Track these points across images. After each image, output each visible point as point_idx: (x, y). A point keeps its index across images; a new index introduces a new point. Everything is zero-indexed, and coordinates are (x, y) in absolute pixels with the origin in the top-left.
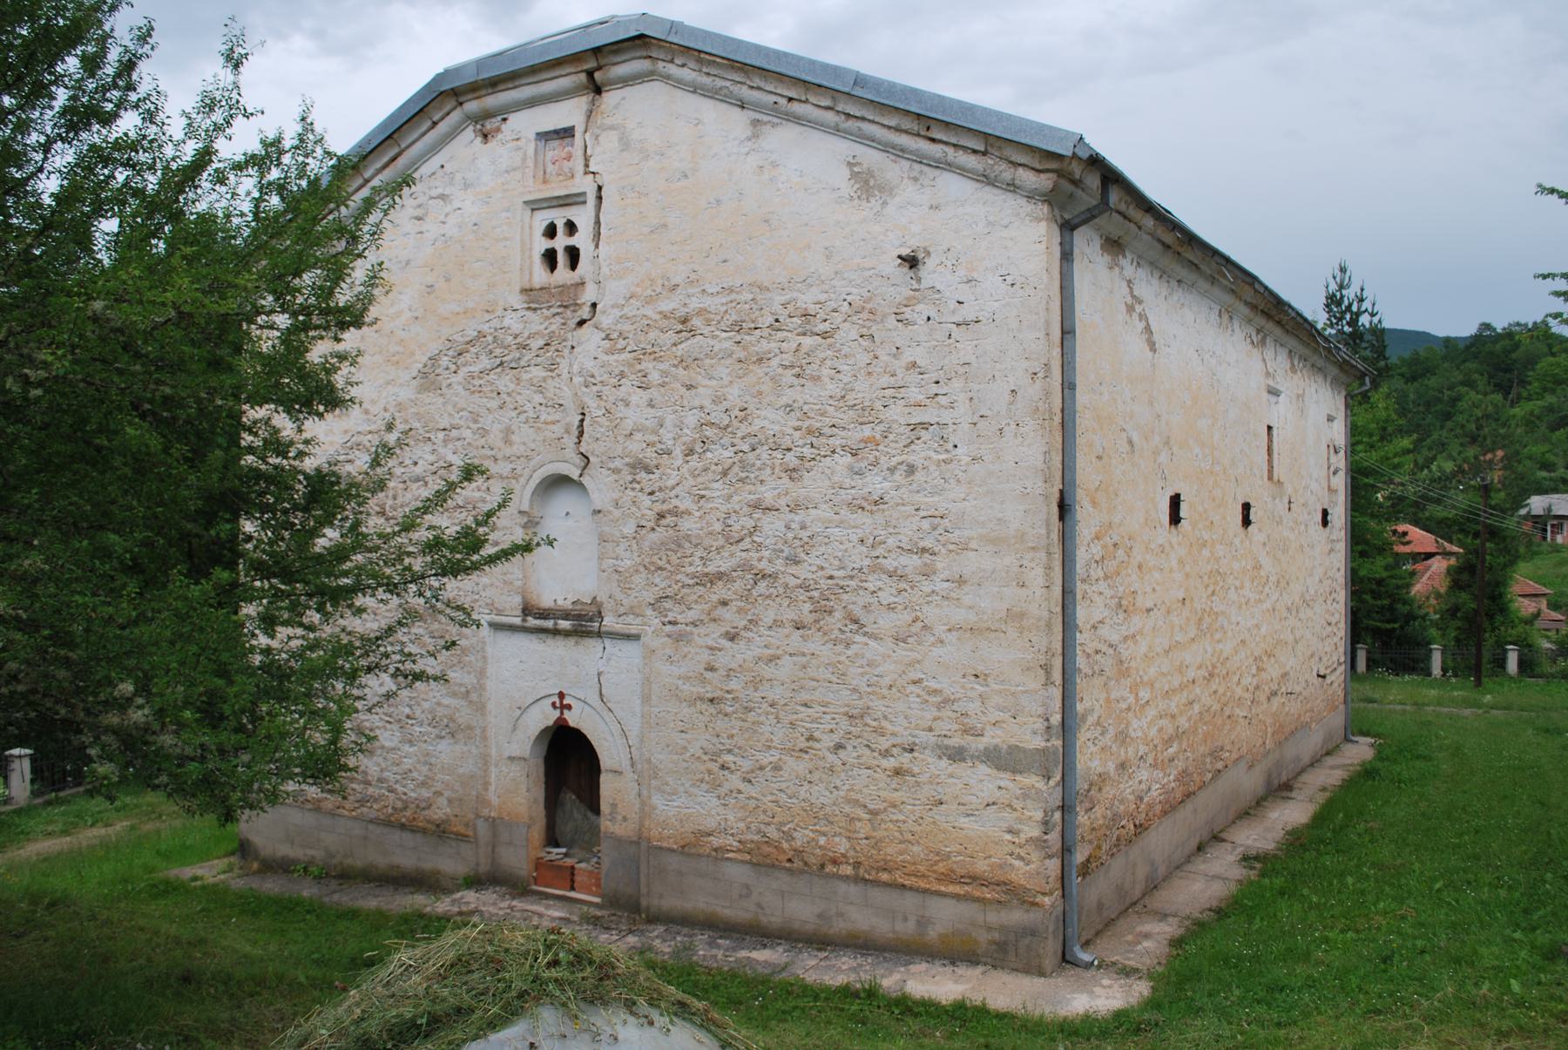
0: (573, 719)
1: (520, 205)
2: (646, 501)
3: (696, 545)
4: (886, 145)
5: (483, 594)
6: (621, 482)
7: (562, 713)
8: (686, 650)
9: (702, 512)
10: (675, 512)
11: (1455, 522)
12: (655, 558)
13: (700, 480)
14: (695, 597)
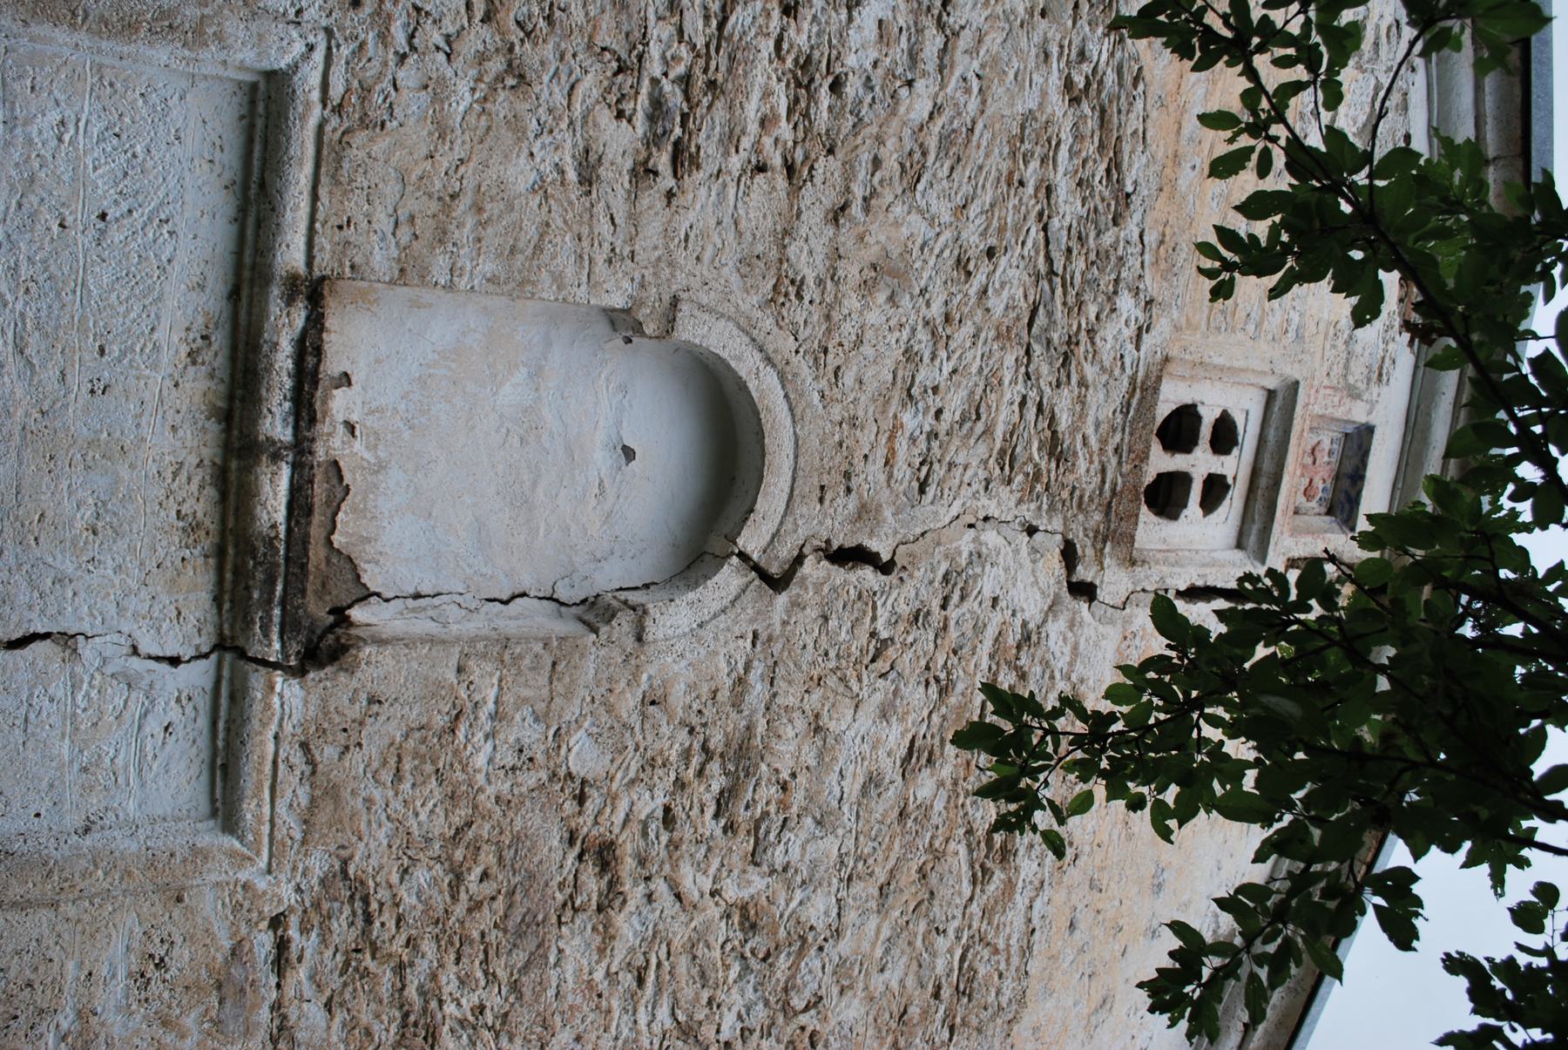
1: (1294, 372)
2: (650, 804)
3: (515, 987)
5: (408, 76)
6: (709, 712)
8: (189, 1021)
9: (603, 986)
10: (612, 896)
12: (488, 858)
13: (683, 962)
14: (365, 1018)
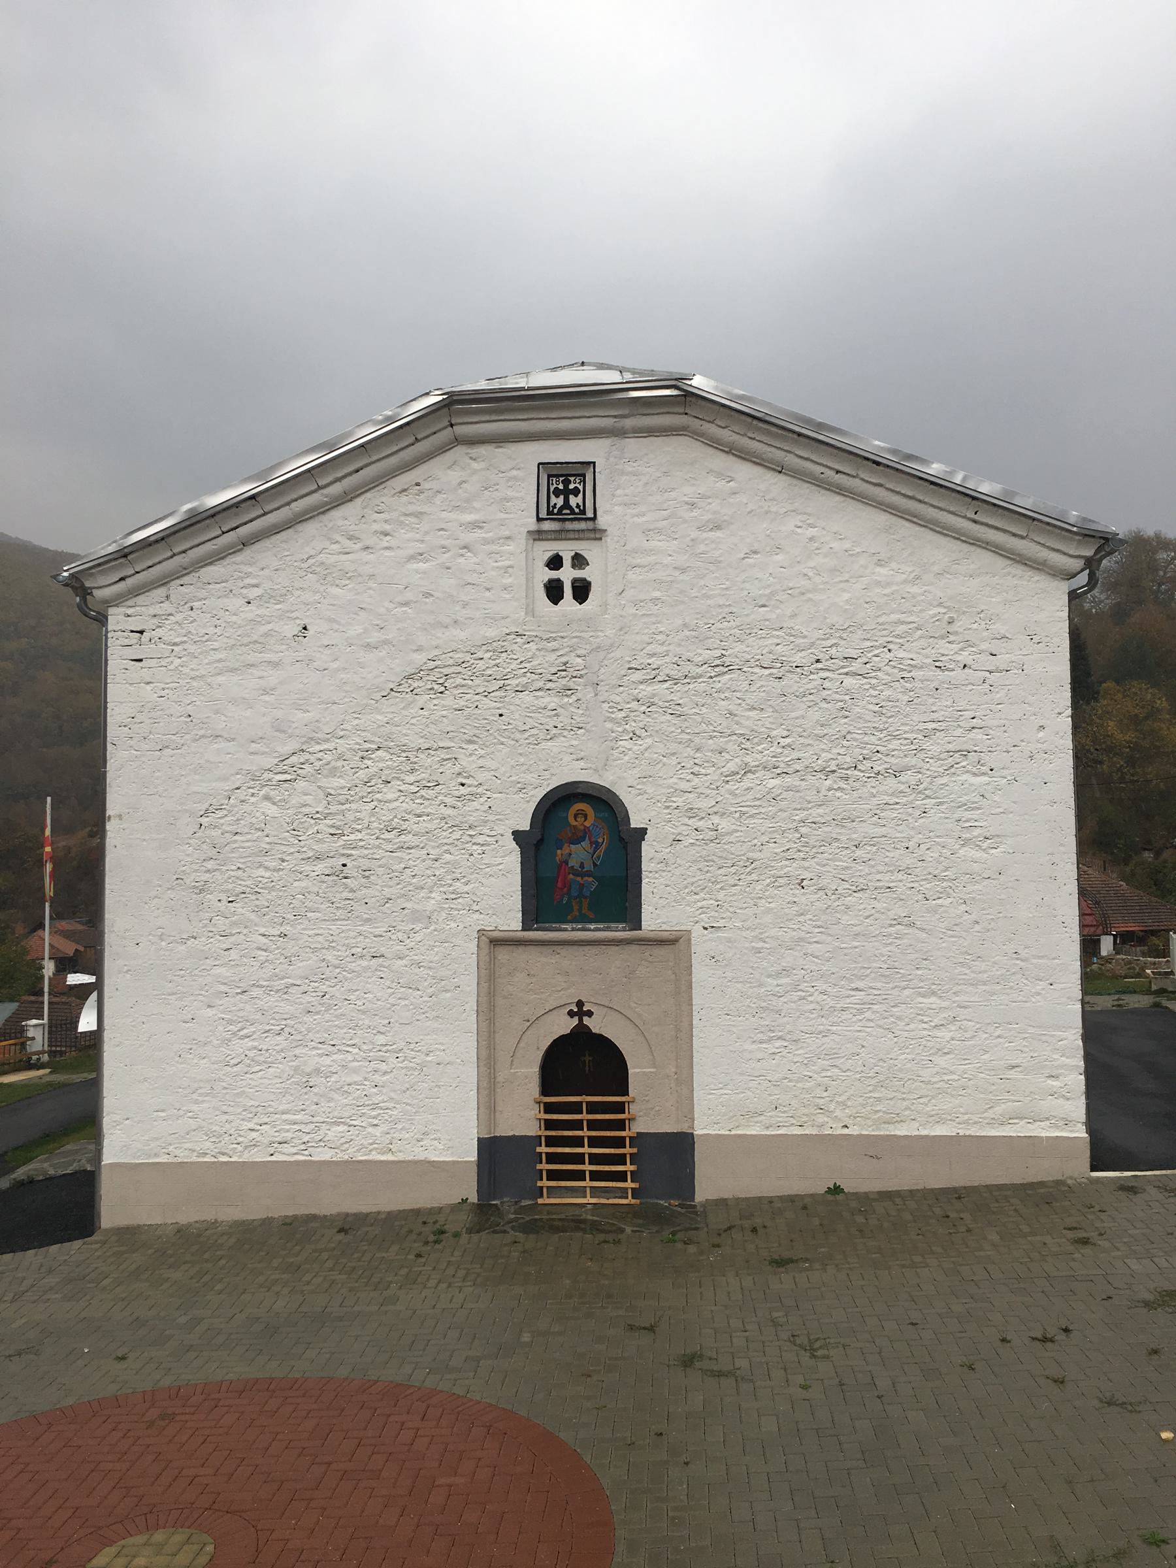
0: (594, 1025)
4: (928, 521)
7: (581, 1020)
11: (842, 1102)
